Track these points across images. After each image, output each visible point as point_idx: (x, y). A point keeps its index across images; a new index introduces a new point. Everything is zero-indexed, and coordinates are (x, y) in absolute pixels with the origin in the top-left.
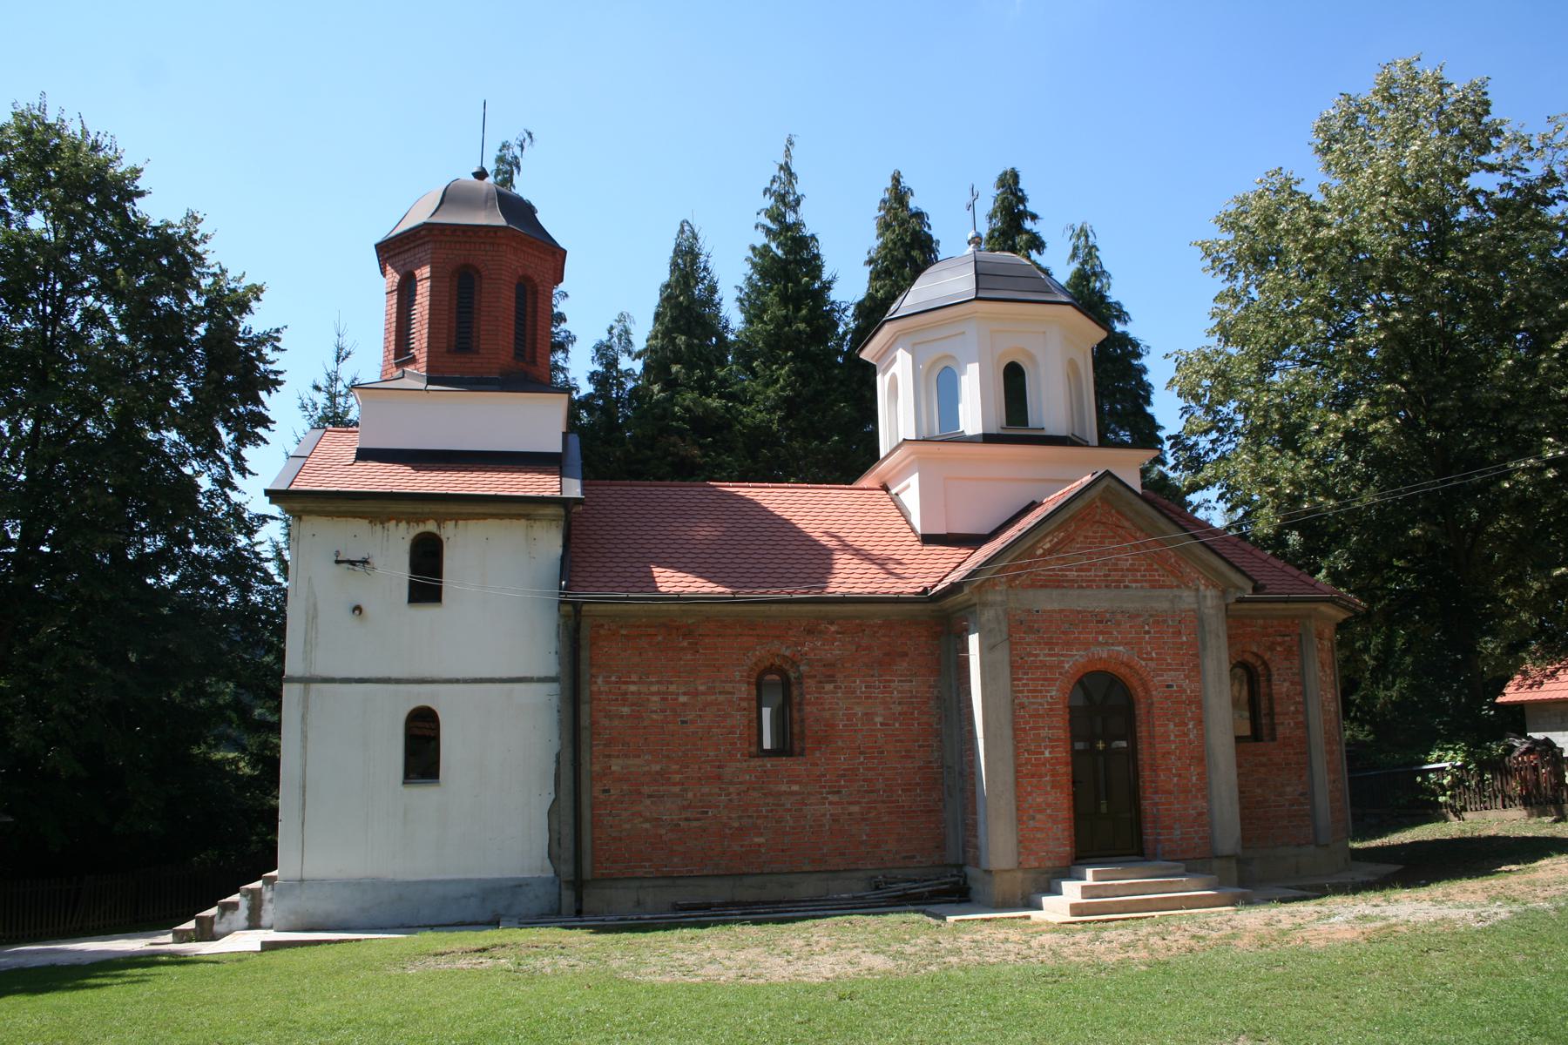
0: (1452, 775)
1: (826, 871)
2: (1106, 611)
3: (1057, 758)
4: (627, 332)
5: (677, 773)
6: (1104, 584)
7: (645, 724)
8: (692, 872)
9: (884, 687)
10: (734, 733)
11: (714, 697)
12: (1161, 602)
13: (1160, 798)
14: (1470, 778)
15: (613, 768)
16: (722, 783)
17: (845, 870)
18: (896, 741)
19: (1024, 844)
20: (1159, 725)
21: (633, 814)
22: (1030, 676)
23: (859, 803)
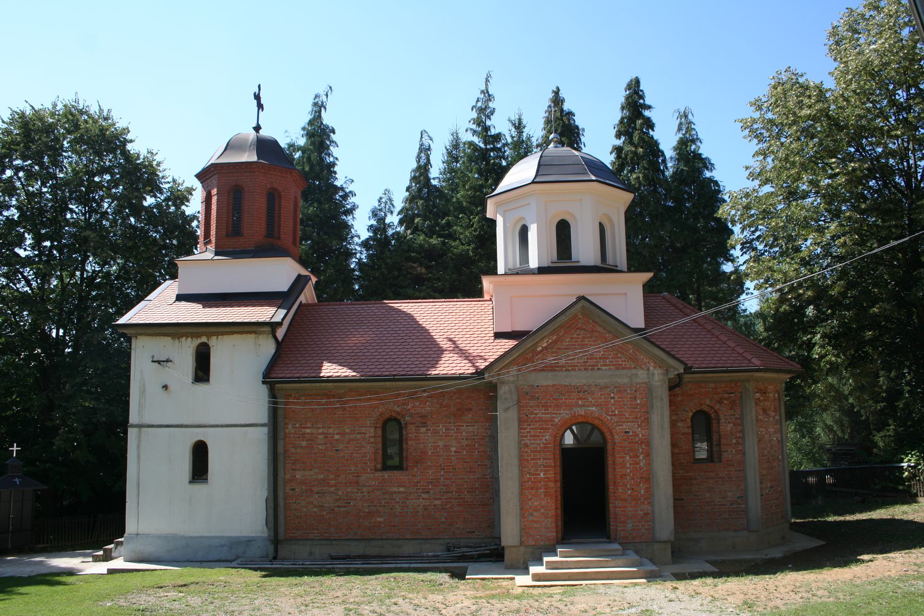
0: (909, 471)
1: (419, 539)
2: (584, 385)
3: (548, 478)
4: (390, 200)
5: (332, 480)
6: (583, 368)
7: (315, 451)
8: (341, 537)
9: (457, 429)
10: (366, 457)
11: (354, 436)
12: (623, 378)
13: (619, 504)
14: (920, 474)
15: (297, 477)
16: (359, 486)
17: (431, 539)
18: (465, 462)
19: (524, 530)
20: (619, 457)
21: (308, 503)
22: (532, 427)
23: (441, 499)
